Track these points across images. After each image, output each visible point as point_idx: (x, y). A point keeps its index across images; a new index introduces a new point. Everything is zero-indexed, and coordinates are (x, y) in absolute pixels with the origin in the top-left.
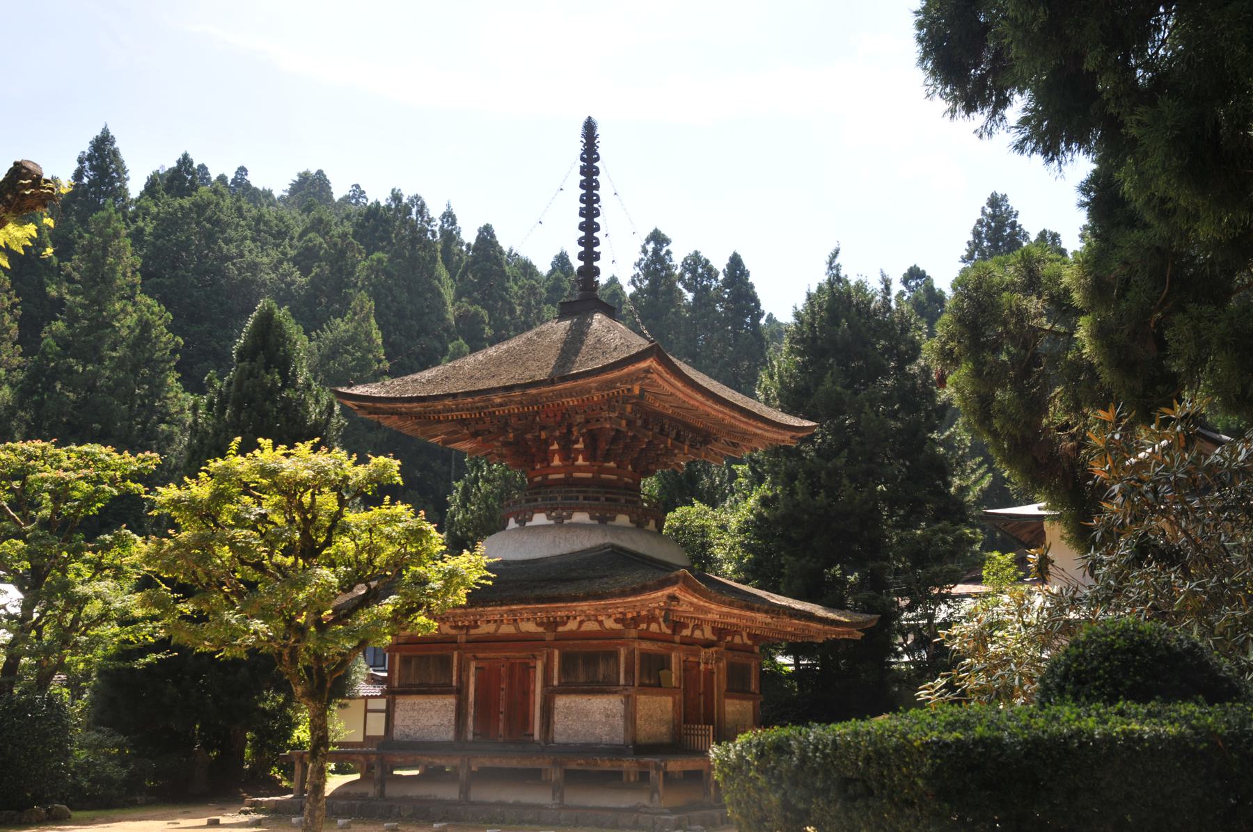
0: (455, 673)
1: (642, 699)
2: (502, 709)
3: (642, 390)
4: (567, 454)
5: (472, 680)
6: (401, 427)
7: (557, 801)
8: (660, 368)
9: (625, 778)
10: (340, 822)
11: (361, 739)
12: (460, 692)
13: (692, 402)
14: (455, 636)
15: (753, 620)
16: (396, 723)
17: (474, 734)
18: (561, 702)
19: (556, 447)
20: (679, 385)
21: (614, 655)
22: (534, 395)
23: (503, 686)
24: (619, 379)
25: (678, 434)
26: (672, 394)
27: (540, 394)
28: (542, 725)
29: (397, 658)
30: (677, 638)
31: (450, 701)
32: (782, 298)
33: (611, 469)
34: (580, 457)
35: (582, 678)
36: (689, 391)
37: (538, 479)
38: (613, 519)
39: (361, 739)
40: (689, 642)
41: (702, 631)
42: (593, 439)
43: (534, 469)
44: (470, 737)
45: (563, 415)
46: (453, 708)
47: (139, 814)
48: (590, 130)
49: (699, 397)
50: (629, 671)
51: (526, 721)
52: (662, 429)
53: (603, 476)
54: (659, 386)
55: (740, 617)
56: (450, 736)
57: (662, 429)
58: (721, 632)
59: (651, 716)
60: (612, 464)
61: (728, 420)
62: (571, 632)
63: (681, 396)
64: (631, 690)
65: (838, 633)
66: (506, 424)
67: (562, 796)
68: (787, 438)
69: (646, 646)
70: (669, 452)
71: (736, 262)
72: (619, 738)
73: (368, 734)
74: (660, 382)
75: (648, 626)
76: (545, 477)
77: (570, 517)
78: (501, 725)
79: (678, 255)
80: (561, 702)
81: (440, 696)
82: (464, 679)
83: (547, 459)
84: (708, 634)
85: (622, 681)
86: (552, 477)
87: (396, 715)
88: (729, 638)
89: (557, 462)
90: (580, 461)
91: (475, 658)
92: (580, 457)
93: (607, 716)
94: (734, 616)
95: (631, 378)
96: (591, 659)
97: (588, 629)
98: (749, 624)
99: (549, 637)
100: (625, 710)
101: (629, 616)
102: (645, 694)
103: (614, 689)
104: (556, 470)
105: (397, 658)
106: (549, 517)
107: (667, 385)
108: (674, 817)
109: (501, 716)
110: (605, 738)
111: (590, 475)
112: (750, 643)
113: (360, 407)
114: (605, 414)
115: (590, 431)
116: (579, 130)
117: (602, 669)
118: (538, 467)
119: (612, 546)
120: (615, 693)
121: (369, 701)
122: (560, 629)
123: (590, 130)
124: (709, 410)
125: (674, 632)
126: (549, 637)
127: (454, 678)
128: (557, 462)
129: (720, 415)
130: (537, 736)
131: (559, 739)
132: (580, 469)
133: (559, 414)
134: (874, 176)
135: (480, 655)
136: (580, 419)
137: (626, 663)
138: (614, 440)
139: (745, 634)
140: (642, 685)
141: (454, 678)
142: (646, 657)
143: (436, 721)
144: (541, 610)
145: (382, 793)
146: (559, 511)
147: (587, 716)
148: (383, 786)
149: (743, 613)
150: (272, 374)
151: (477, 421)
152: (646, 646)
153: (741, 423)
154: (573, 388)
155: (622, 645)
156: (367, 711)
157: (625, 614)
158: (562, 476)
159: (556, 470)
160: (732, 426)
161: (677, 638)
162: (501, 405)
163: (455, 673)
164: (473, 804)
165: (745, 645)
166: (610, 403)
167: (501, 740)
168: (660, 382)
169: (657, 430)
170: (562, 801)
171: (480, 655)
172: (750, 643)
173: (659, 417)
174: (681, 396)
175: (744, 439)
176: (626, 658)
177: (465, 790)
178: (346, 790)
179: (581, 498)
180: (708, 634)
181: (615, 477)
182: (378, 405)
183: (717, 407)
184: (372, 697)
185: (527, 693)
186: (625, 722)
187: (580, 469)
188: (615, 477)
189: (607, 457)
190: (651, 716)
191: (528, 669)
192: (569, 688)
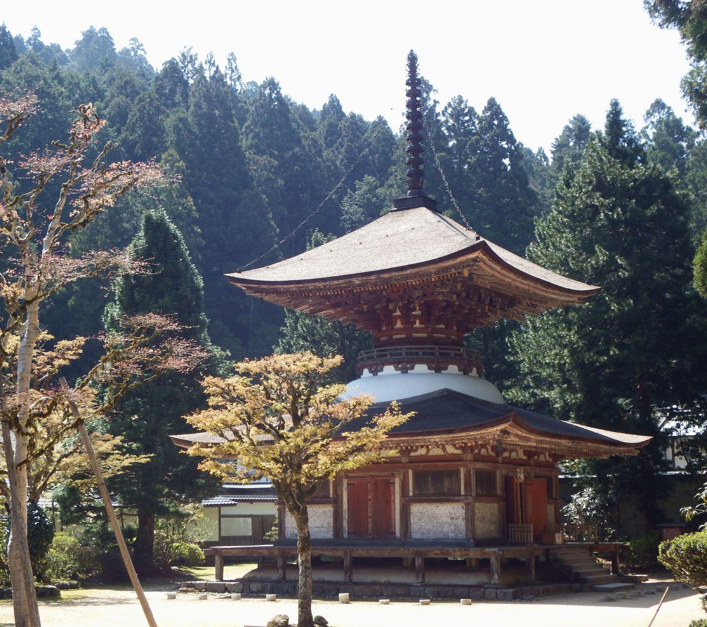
0: (331, 488)
1: (478, 505)
2: (370, 514)
3: (471, 274)
4: (407, 318)
5: (345, 493)
6: (276, 301)
8: (485, 257)
9: (468, 565)
11: (217, 539)
12: (336, 502)
13: (506, 280)
15: (558, 444)
16: (287, 525)
17: (349, 533)
18: (416, 509)
19: (398, 313)
20: (498, 268)
21: (457, 473)
22: (387, 279)
23: (370, 497)
24: (454, 266)
25: (491, 300)
26: (493, 275)
27: (390, 278)
30: (500, 459)
31: (329, 509)
32: (537, 132)
33: (441, 329)
34: (418, 321)
35: (431, 491)
36: (505, 272)
37: (384, 338)
38: (446, 369)
39: (217, 539)
40: (509, 462)
41: (517, 453)
42: (428, 308)
43: (380, 331)
45: (405, 290)
48: (413, 60)
49: (512, 276)
50: (468, 485)
52: (480, 298)
53: (435, 335)
54: (483, 270)
55: (549, 443)
56: (330, 535)
57: (480, 298)
58: (529, 453)
59: (484, 518)
60: (442, 326)
61: (532, 290)
62: (421, 456)
63: (499, 276)
64: (470, 500)
65: (621, 452)
67: (423, 577)
68: (576, 299)
69: (479, 465)
70: (484, 315)
71: (493, 107)
72: (462, 535)
74: (484, 267)
76: (390, 338)
77: (412, 368)
79: (441, 99)
80: (416, 509)
81: (321, 506)
82: (339, 492)
83: (391, 322)
84: (522, 456)
85: (463, 493)
86: (395, 337)
88: (536, 457)
89: (399, 325)
90: (417, 324)
92: (418, 321)
93: (452, 519)
94: (546, 442)
95: (463, 265)
96: (438, 476)
98: (557, 447)
99: (404, 460)
100: (466, 513)
101: (469, 445)
102: (480, 502)
103: (457, 498)
104: (399, 331)
107: (488, 268)
108: (511, 591)
109: (370, 520)
110: (451, 535)
111: (425, 335)
112: (550, 460)
113: (249, 288)
114: (438, 290)
115: (426, 302)
116: (405, 62)
117: (447, 484)
118: (384, 328)
120: (458, 501)
121: (222, 508)
122: (413, 454)
123: (413, 60)
124: (519, 284)
126: (404, 460)
127: (331, 492)
128: (399, 325)
129: (527, 287)
130: (398, 534)
131: (416, 536)
132: (417, 330)
133: (402, 290)
134: (641, 74)
136: (418, 293)
137: (465, 480)
138: (445, 308)
139: (547, 454)
140: (478, 495)
141: (331, 492)
142: (479, 474)
144: (403, 442)
146: (404, 365)
147: (436, 518)
149: (553, 440)
152: (479, 465)
153: (541, 291)
154: (416, 273)
155: (462, 466)
156: (220, 516)
157: (466, 444)
158: (403, 336)
159: (399, 331)
160: (535, 294)
161: (532, 462)
162: (360, 285)
163: (331, 488)
164: (355, 583)
165: (490, 456)
166: (442, 282)
167: (370, 537)
168: (484, 267)
169: (476, 299)
172: (550, 460)
173: (478, 289)
174: (499, 276)
175: (542, 302)
176: (465, 475)
178: (252, 575)
179: (421, 354)
180: (522, 456)
181: (444, 336)
182: (263, 286)
183: (525, 282)
184: (225, 505)
185: (389, 502)
186: (467, 523)
187: (417, 330)
188: (444, 336)
189: (439, 321)
190: (484, 518)
191: (389, 484)
192: (423, 497)
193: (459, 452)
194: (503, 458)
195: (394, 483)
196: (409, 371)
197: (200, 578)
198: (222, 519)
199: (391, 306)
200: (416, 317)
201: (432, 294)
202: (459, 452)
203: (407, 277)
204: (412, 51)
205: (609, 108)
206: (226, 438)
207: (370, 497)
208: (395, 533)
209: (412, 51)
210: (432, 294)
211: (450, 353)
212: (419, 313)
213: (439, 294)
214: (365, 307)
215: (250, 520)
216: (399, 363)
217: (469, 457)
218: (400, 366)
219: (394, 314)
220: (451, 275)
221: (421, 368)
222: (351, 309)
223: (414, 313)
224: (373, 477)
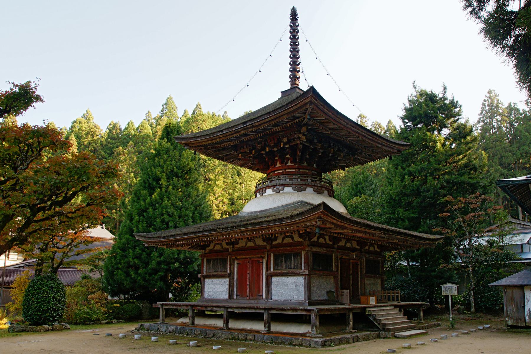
2: (248, 283)
7: (267, 329)
10: (153, 338)
14: (228, 249)
17: (237, 296)
18: (274, 279)
29: (205, 260)
30: (336, 246)
34: (289, 161)
44: (235, 297)
46: (228, 283)
48: (294, 16)
51: (259, 289)
75: (369, 248)
78: (248, 290)
82: (232, 269)
87: (205, 286)
88: (367, 248)
89: (278, 165)
91: (237, 259)
92: (289, 161)
93: (296, 286)
97: (287, 242)
105: (205, 260)
106: (273, 190)
109: (248, 287)
119: (302, 201)
122: (274, 243)
123: (294, 16)
125: (334, 244)
132: (290, 167)
135: (238, 257)
143: (221, 289)
145: (193, 323)
148: (194, 319)
161: (336, 246)
171: (238, 257)
177: (227, 323)
187: (290, 167)
194: (338, 246)
195: (263, 262)
196: (281, 192)
197: (393, 308)
204: (294, 7)
205: (290, 13)
207: (248, 272)
209: (294, 7)
215: (313, 281)
216: (274, 186)
221: (310, 190)
224: (250, 258)
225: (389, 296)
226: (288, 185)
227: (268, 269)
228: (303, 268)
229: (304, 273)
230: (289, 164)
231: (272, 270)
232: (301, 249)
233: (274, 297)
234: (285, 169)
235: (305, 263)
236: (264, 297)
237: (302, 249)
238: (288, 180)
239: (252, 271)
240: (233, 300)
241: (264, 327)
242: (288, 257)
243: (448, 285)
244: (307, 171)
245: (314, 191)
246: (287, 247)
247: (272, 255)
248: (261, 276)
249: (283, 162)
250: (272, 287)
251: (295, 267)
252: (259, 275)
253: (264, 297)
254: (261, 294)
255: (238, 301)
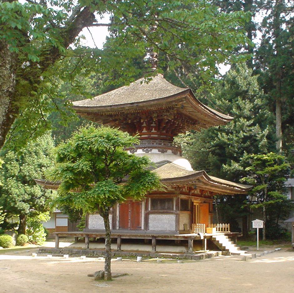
17: (119, 227)
18: (151, 216)
19: (144, 125)
24: (175, 101)
28: (145, 224)
34: (153, 129)
38: (166, 152)
44: (118, 228)
47: (163, 247)
51: (139, 223)
66: (127, 117)
67: (155, 249)
73: (57, 226)
77: (151, 150)
80: (151, 216)
87: (89, 220)
92: (153, 129)
100: (176, 218)
103: (172, 211)
109: (129, 221)
120: (172, 213)
132: (153, 133)
150: (215, 140)
151: (115, 115)
166: (168, 110)
170: (155, 250)
177: (119, 247)
193: (173, 190)
195: (141, 204)
196: (150, 152)
198: (57, 219)
199: (142, 121)
200: (152, 127)
201: (162, 116)
202: (173, 190)
203: (151, 106)
206: (163, 29)
208: (141, 227)
210: (162, 116)
211: (49, 238)
212: (155, 125)
213: (165, 115)
214: (130, 121)
216: (145, 148)
217: (178, 192)
218: (145, 149)
219: (143, 125)
220: (172, 106)
222: (122, 122)
223: (152, 125)
225: (219, 228)
226: (155, 148)
227: (146, 208)
228: (174, 209)
229: (176, 213)
230: (153, 131)
231: (149, 209)
232: (173, 196)
233: (150, 229)
234: (150, 135)
235: (176, 206)
236: (143, 228)
237: (174, 196)
238: (155, 144)
239: (132, 210)
240: (115, 230)
241: (152, 249)
242: (163, 201)
243: (257, 220)
244: (165, 137)
245: (172, 152)
246: (162, 194)
247: (150, 199)
248: (140, 214)
249: (149, 128)
250: (150, 222)
251: (169, 208)
252: (139, 213)
253: (143, 228)
254: (140, 226)
255: (121, 231)
